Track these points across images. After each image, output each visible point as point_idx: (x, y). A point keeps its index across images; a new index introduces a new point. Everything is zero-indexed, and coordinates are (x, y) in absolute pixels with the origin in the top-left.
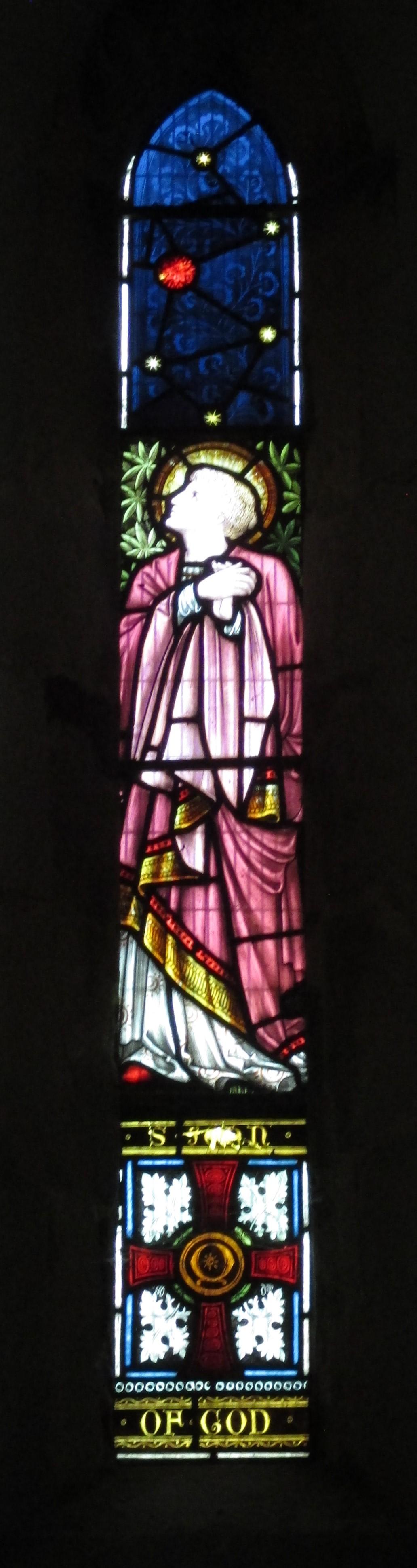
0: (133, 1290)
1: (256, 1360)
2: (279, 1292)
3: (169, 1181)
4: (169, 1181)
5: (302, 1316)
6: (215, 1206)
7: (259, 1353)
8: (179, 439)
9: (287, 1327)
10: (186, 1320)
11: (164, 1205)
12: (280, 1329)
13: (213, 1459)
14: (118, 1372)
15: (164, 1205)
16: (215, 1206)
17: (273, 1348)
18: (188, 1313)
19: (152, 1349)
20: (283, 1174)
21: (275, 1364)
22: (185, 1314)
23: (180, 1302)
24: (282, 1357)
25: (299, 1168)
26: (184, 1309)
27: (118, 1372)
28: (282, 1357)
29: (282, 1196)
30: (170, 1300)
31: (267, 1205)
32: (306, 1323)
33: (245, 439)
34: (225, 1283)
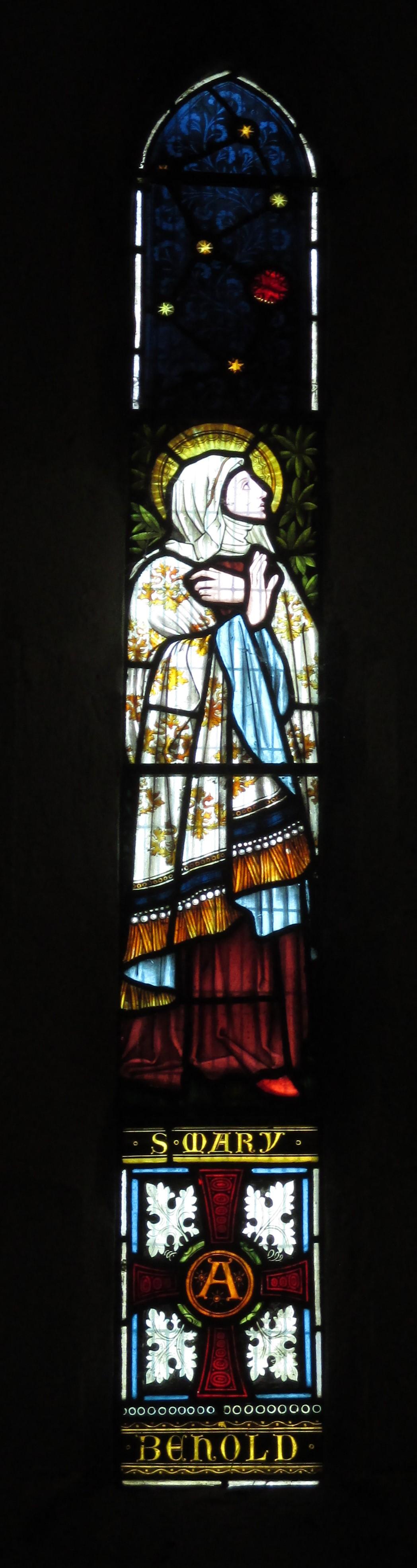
0: (301, 1256)
1: (269, 1382)
2: (153, 1253)
3: (269, 1374)
4: (269, 1374)
5: (314, 1329)
6: (221, 1220)
7: (172, 1190)
8: (188, 405)
9: (145, 1217)
10: (248, 1224)
11: (274, 1348)
12: (293, 1349)
13: (218, 1404)
14: (316, 1172)
15: (170, 1218)
16: (221, 1220)
17: (286, 1368)
18: (245, 1231)
19: (282, 1194)
20: (290, 1186)
21: (288, 1386)
22: (248, 1231)
23: (252, 1242)
24: (149, 1187)
25: (309, 1175)
26: (249, 1236)
27: (316, 1172)
28: (149, 1187)
29: (289, 1209)
30: (264, 1244)
31: (271, 1217)
32: (318, 1336)
33: (259, 413)
34: (209, 1261)
